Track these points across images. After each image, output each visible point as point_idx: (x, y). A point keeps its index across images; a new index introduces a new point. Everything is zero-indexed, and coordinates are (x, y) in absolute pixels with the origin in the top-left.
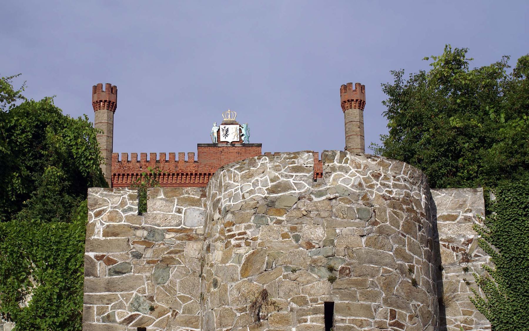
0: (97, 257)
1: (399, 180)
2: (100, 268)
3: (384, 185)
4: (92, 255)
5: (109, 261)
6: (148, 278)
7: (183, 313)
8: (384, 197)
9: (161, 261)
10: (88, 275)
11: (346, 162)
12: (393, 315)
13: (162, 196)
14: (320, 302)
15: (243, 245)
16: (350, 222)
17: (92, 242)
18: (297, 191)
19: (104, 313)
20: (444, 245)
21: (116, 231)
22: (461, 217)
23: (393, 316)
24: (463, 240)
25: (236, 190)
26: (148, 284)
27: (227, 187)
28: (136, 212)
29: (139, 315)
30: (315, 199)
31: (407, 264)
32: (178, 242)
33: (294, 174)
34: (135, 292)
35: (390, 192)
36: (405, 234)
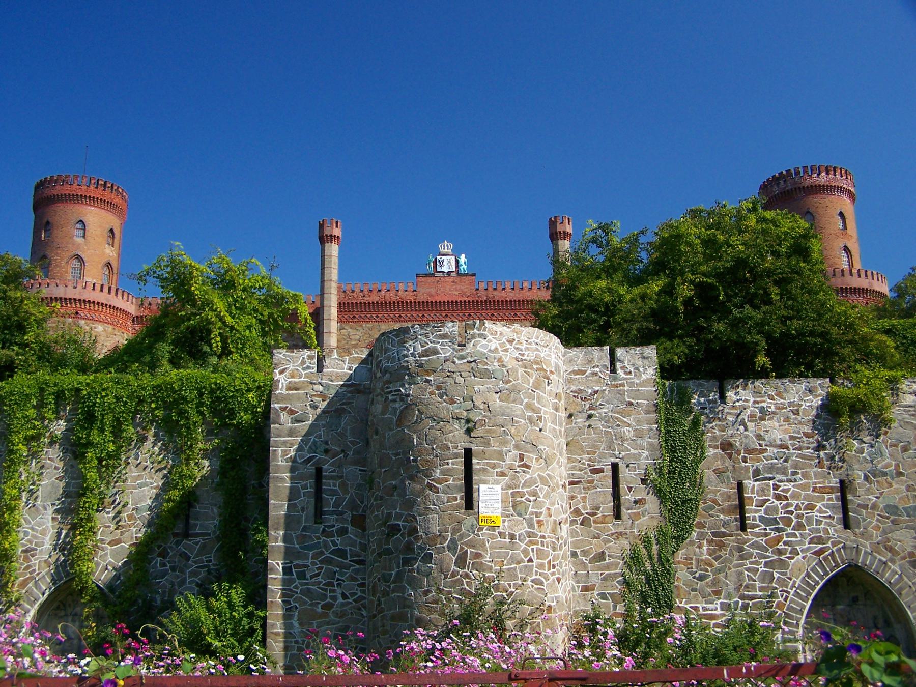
0: (281, 408)
1: (530, 344)
2: (284, 417)
3: (518, 348)
4: (277, 406)
5: (292, 412)
6: (324, 426)
7: (353, 454)
8: (517, 359)
9: (335, 411)
11: (484, 330)
12: (521, 458)
13: (336, 356)
14: (459, 448)
15: (398, 400)
17: (277, 396)
18: (443, 355)
19: (287, 455)
20: (574, 396)
21: (296, 386)
22: (589, 372)
23: (522, 459)
24: (590, 391)
25: (393, 353)
27: (387, 350)
28: (315, 370)
30: (457, 362)
31: (535, 415)
32: (349, 395)
33: (441, 341)
34: (313, 438)
35: (523, 355)
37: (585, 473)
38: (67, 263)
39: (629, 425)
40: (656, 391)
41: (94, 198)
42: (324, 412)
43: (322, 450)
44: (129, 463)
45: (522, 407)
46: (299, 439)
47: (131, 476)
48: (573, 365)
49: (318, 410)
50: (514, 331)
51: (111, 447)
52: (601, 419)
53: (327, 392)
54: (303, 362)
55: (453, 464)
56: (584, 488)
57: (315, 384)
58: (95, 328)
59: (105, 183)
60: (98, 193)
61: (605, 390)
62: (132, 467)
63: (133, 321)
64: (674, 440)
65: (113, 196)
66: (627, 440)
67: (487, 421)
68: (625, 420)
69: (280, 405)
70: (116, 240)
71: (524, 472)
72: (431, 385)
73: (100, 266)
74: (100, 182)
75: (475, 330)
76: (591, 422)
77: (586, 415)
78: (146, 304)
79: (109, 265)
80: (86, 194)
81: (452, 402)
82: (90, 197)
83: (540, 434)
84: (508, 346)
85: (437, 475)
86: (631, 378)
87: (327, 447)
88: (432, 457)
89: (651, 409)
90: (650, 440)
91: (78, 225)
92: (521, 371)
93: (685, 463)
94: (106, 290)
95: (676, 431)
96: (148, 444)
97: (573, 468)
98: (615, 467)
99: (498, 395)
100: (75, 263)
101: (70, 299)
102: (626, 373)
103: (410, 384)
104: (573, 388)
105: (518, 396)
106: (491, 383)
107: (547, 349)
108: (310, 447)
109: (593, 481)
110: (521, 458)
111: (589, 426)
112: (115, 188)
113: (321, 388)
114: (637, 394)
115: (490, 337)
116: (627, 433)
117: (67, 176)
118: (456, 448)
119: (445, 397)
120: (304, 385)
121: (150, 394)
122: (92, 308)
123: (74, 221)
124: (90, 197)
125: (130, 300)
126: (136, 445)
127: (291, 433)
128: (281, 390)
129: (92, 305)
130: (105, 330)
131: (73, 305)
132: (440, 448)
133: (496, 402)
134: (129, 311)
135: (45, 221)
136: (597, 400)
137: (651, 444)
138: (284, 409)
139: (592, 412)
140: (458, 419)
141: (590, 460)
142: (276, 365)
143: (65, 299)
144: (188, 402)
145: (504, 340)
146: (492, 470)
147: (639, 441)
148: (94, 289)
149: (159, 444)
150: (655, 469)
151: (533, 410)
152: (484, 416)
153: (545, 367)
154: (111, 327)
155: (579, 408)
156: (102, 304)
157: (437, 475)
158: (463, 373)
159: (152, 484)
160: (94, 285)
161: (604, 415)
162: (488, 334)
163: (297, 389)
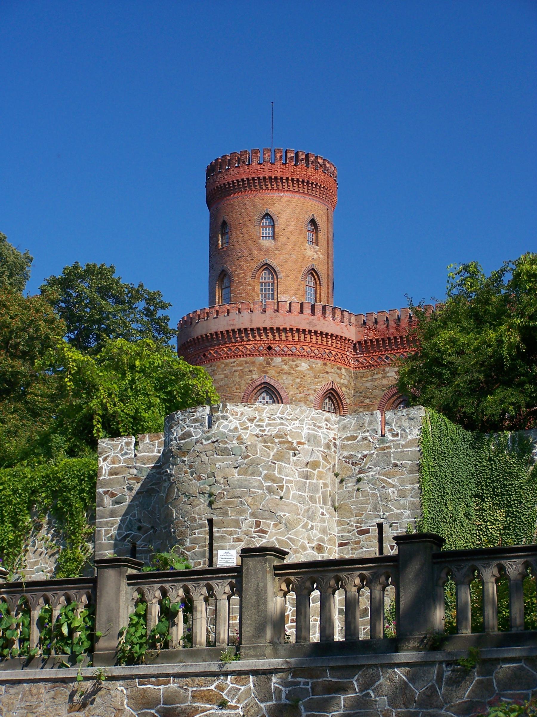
0: (104, 492)
2: (107, 501)
3: (259, 426)
5: (113, 495)
8: (257, 436)
9: (146, 492)
10: (99, 507)
11: (226, 412)
12: (258, 524)
14: (203, 519)
16: (227, 458)
18: (195, 438)
19: (109, 534)
20: (346, 462)
21: (116, 471)
22: (360, 437)
24: (360, 456)
26: (137, 510)
29: (132, 533)
30: (205, 443)
31: (275, 485)
34: (129, 517)
35: (263, 431)
36: (275, 462)
37: (353, 535)
38: (254, 277)
39: (393, 486)
40: (419, 451)
41: (282, 178)
42: (138, 493)
43: (136, 528)
44: (27, 551)
45: (260, 478)
46: (119, 519)
47: (30, 562)
48: (346, 432)
49: (134, 491)
50: (255, 410)
51: (11, 536)
52: (369, 482)
53: (140, 475)
54: (122, 449)
55: (199, 534)
56: (352, 549)
57: (131, 468)
58: (297, 366)
59: (297, 154)
60: (289, 171)
61: (373, 454)
62: (31, 554)
63: (355, 348)
64: (510, 495)
65: (310, 171)
66: (391, 500)
67: (225, 493)
68: (390, 481)
69: (103, 490)
70: (322, 236)
71: (260, 537)
72: (186, 465)
73: (300, 275)
74: (289, 155)
75: (219, 413)
76: (360, 485)
77: (355, 479)
78: (370, 323)
79: (313, 272)
80: (270, 175)
81: (199, 478)
82: (276, 178)
83: (281, 502)
84: (249, 424)
85: (188, 544)
86: (397, 440)
87: (140, 524)
88: (184, 529)
89: (414, 469)
90: (412, 499)
91: (264, 221)
92: (260, 446)
93: (520, 518)
94: (307, 310)
95: (512, 485)
96: (43, 532)
97: (342, 531)
98: (380, 526)
99: (237, 470)
100: (265, 275)
101: (258, 329)
102: (393, 435)
103: (173, 465)
104: (346, 454)
105: (256, 469)
106: (230, 459)
107: (298, 422)
108: (127, 526)
109: (359, 542)
110: (258, 524)
111: (358, 490)
112: (312, 159)
113: (135, 471)
114: (402, 455)
115: (231, 418)
116: (391, 494)
117: (243, 153)
118: (201, 519)
119: (195, 475)
120: (122, 470)
121: (39, 485)
122: (290, 338)
123: (259, 215)
124: (276, 178)
125: (346, 320)
126: (33, 533)
127: (112, 514)
128: (104, 476)
129: (290, 334)
130: (311, 368)
131: (264, 337)
132: (190, 520)
133: (235, 476)
134: (346, 335)
135: (220, 222)
136: (366, 464)
137: (413, 503)
138: (106, 493)
139: (361, 476)
140: (203, 493)
141: (357, 522)
142: (100, 453)
143: (252, 329)
144: (70, 490)
145: (244, 419)
146: (229, 537)
147: (403, 501)
148: (302, 311)
149: (52, 531)
150: (416, 527)
151: (274, 481)
152: (224, 490)
153: (290, 440)
154: (320, 362)
155: (349, 473)
156: (304, 331)
157: (188, 544)
158: (207, 452)
159: (46, 568)
160: (302, 305)
161: (371, 477)
162: (229, 415)
163: (116, 474)
